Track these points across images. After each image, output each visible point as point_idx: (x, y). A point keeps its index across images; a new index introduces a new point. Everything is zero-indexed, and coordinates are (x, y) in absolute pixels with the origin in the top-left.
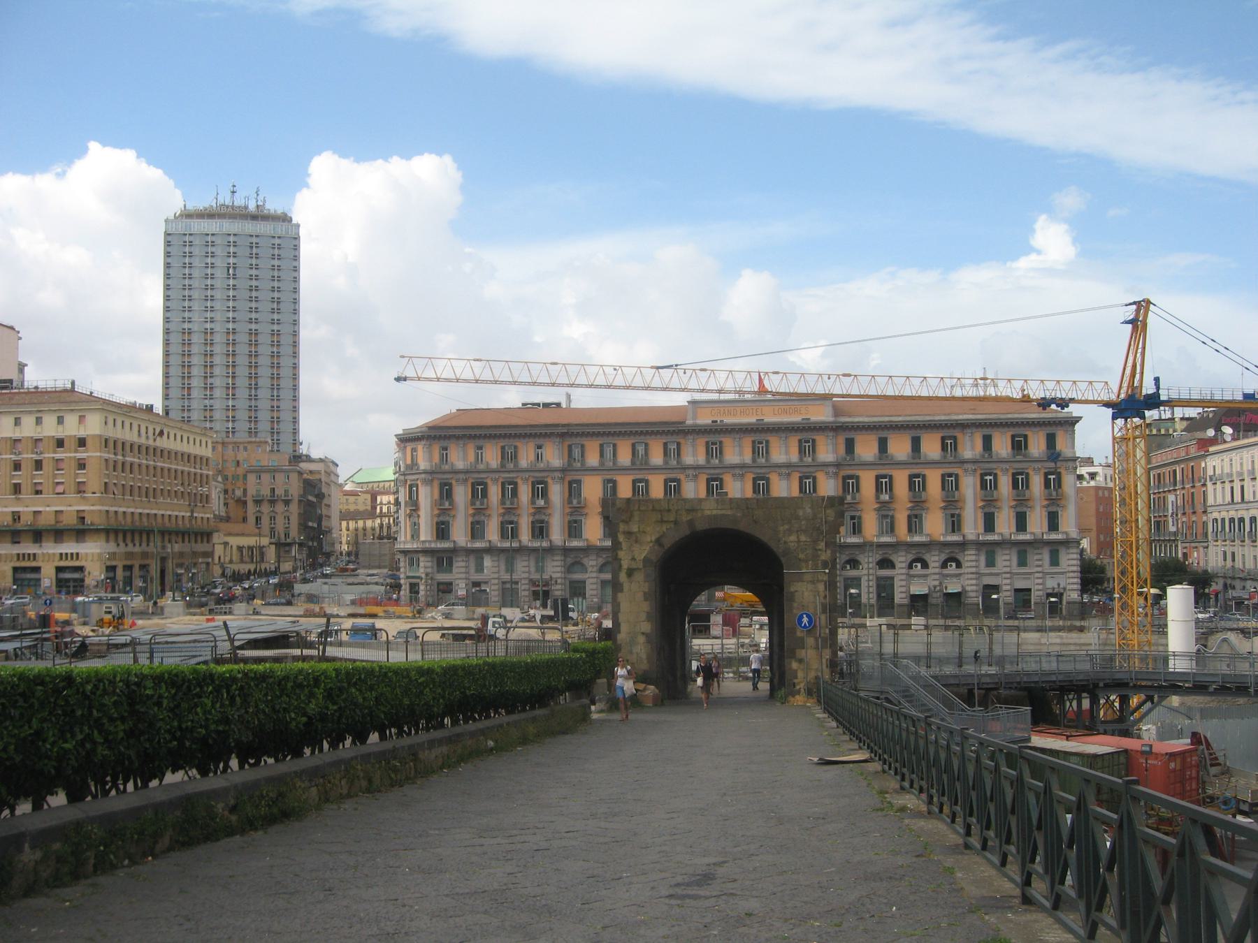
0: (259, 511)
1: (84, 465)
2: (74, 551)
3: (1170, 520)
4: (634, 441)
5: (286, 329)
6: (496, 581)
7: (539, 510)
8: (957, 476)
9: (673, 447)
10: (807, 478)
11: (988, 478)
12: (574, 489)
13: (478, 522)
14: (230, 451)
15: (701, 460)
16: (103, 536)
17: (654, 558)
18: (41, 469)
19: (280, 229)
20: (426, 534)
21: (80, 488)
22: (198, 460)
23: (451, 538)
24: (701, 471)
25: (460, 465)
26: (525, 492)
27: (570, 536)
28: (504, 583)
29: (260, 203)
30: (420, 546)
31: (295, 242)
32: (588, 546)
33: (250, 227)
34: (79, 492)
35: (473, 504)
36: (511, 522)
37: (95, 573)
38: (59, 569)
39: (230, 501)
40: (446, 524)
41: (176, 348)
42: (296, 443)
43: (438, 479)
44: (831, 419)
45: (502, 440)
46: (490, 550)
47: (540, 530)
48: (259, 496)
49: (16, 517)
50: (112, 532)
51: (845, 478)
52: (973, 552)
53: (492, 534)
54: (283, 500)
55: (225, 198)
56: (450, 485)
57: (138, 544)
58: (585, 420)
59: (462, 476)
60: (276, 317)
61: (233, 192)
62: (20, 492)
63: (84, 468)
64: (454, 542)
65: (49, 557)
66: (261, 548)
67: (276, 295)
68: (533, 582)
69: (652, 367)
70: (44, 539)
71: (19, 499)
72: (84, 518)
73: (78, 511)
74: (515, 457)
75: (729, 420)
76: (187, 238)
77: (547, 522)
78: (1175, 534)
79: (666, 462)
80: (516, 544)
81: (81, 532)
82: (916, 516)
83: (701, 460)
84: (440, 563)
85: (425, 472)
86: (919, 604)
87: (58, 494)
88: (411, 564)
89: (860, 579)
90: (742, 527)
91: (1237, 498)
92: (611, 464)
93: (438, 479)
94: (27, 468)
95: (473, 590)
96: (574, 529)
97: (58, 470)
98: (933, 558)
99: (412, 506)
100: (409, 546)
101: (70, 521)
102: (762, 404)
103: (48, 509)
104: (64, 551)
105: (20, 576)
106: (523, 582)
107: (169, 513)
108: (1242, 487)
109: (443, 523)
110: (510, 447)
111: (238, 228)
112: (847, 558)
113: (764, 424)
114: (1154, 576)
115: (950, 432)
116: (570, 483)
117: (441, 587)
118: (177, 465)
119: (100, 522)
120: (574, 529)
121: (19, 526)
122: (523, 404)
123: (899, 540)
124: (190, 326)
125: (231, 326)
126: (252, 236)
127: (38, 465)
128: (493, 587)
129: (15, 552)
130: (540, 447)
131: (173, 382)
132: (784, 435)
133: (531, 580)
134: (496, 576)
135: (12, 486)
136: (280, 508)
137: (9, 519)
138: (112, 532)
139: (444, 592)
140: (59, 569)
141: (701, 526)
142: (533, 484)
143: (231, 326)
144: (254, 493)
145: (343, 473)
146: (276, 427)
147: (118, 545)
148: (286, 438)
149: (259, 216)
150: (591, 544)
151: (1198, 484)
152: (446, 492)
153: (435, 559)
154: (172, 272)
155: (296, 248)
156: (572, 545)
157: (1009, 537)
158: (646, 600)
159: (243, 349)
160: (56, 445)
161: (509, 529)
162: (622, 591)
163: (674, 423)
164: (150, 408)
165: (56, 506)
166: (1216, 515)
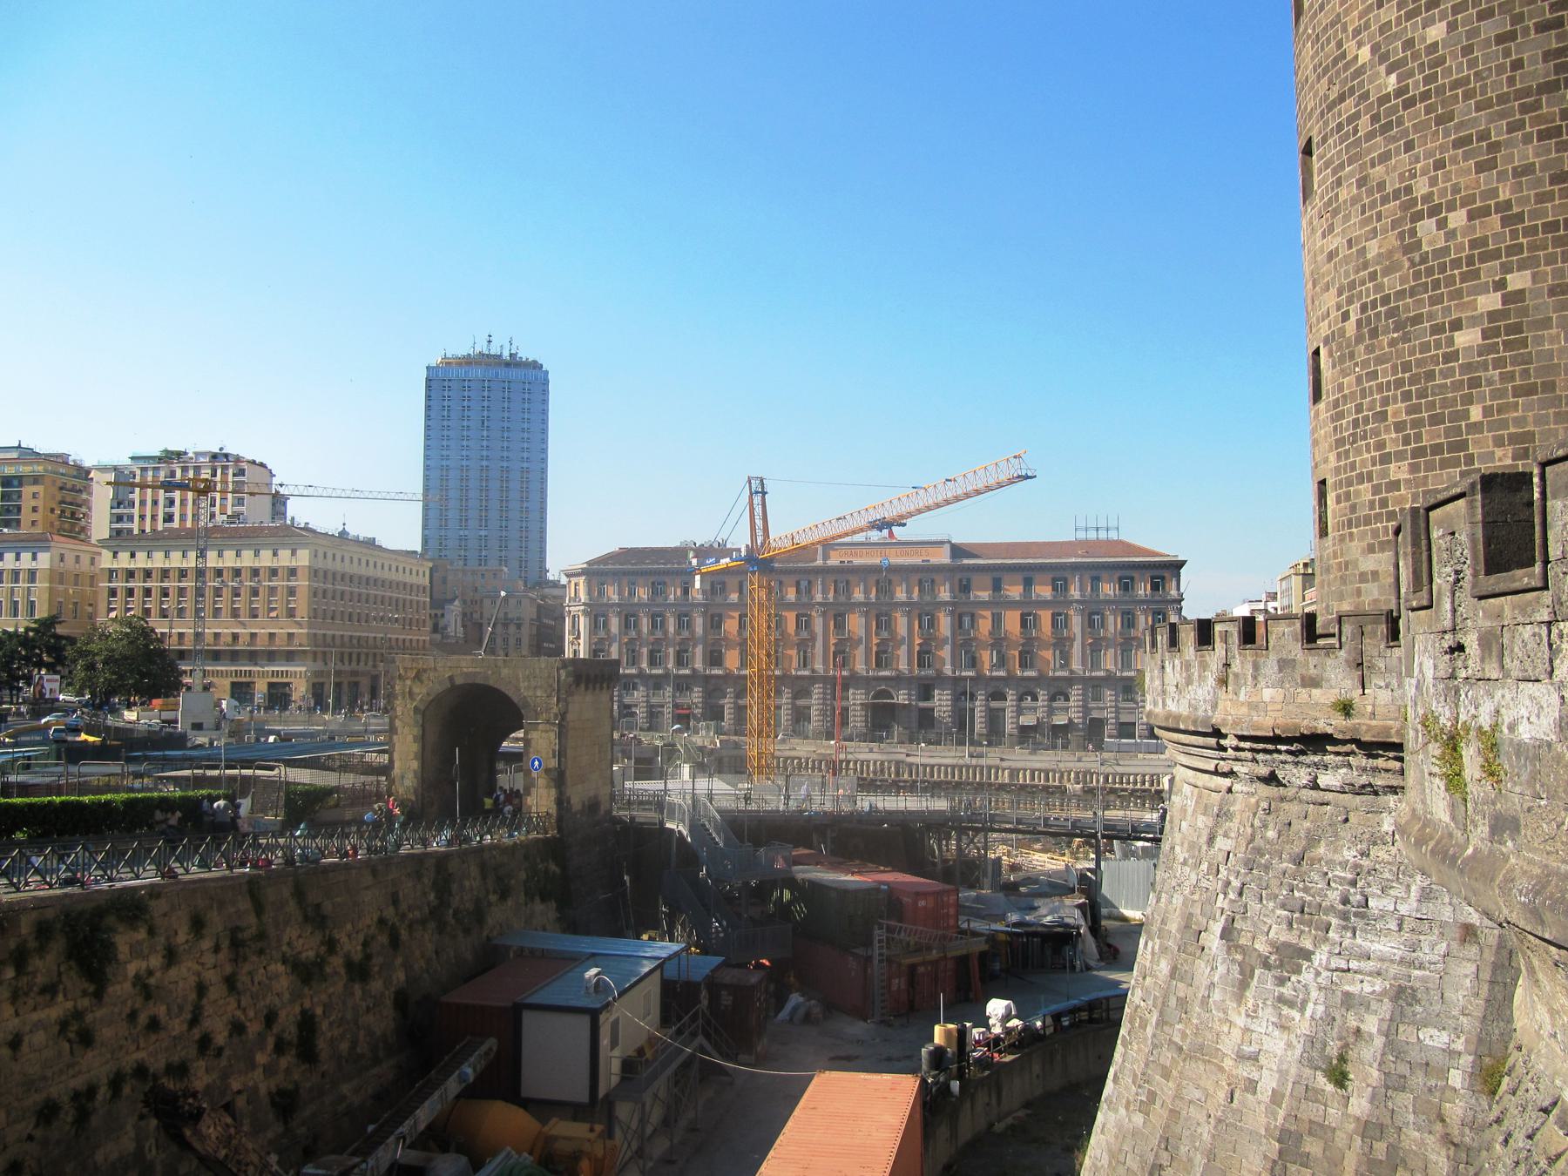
9: (804, 584)
11: (1096, 617)
19: (531, 373)
33: (503, 373)
37: (300, 690)
38: (271, 685)
39: (469, 623)
51: (712, 616)
55: (481, 347)
57: (347, 663)
76: (446, 384)
82: (1028, 652)
86: (1025, 734)
90: (491, 683)
114: (587, 688)
115: (1059, 576)
116: (712, 616)
124: (448, 463)
125: (484, 463)
136: (512, 629)
137: (230, 639)
140: (271, 685)
143: (484, 463)
149: (514, 363)
154: (433, 414)
155: (545, 392)
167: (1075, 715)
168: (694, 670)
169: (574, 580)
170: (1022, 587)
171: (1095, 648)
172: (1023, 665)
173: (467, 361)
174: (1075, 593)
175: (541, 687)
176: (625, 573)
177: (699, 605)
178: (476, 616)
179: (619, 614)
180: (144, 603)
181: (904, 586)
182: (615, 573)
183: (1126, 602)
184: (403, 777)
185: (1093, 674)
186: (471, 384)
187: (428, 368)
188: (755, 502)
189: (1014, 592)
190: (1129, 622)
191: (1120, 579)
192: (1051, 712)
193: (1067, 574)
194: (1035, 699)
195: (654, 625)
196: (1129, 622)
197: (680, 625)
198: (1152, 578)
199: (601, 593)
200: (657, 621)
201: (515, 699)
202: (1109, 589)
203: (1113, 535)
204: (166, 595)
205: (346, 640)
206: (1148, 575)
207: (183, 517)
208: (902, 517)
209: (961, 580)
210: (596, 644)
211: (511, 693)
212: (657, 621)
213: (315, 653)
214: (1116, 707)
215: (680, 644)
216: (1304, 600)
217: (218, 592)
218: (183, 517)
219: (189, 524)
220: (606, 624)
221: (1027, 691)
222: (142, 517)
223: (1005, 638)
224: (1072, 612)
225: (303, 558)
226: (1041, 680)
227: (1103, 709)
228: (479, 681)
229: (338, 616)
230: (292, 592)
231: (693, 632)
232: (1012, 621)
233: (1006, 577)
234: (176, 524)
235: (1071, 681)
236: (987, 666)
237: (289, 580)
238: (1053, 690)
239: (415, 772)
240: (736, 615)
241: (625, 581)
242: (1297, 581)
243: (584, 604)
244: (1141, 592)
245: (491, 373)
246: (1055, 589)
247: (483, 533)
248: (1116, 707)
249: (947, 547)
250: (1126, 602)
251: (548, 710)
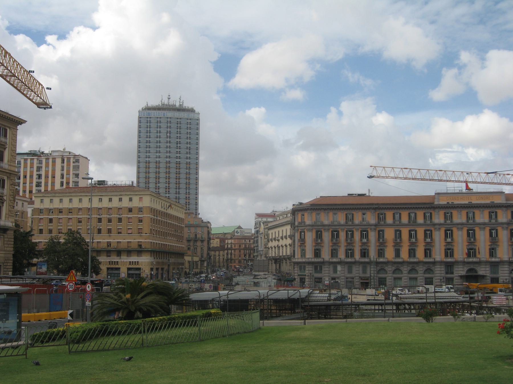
0: (189, 245)
1: (142, 220)
2: (136, 261)
4: (409, 212)
6: (343, 278)
7: (364, 244)
8: (431, 231)
9: (397, 216)
10: (493, 230)
12: (381, 234)
13: (335, 249)
15: (442, 221)
16: (149, 253)
18: (121, 222)
19: (191, 115)
20: (309, 255)
21: (140, 231)
22: (180, 219)
23: (321, 257)
24: (442, 226)
25: (326, 222)
26: (357, 236)
27: (379, 256)
28: (347, 278)
29: (181, 104)
30: (307, 260)
31: (197, 121)
32: (388, 261)
33: (177, 114)
34: (139, 233)
35: (332, 241)
36: (350, 250)
38: (129, 269)
40: (319, 250)
43: (315, 229)
44: (505, 202)
45: (346, 211)
46: (340, 263)
47: (364, 253)
48: (189, 238)
49: (109, 244)
50: (155, 252)
52: (461, 267)
53: (342, 255)
54: (200, 240)
56: (321, 232)
58: (403, 202)
59: (327, 227)
60: (188, 156)
61: (169, 98)
62: (111, 233)
63: (142, 222)
64: (323, 259)
65: (124, 263)
67: (188, 146)
68: (361, 278)
69: (485, 173)
70: (122, 255)
71: (110, 236)
72: (141, 245)
73: (138, 242)
75: (456, 202)
76: (149, 119)
77: (368, 250)
79: (425, 222)
80: (353, 260)
81: (140, 251)
83: (442, 221)
84: (316, 268)
85: (309, 225)
87: (129, 234)
88: (300, 269)
89: (453, 278)
92: (398, 222)
93: (315, 229)
94: (115, 222)
95: (332, 282)
96: (381, 253)
97: (129, 223)
98: (420, 269)
99: (302, 241)
100: (300, 260)
101: (134, 246)
102: (471, 194)
103: (124, 241)
104: (131, 261)
105: (130, 272)
106: (356, 278)
109: (317, 250)
110: (350, 214)
111: (172, 115)
112: (380, 268)
113: (495, 204)
116: (379, 231)
117: (316, 280)
118: (173, 222)
119: (149, 247)
120: (381, 253)
121: (109, 248)
122: (348, 195)
123: (456, 260)
124: (150, 159)
126: (178, 118)
127: (120, 220)
128: (342, 280)
129: (108, 261)
130: (364, 214)
132: (459, 210)
133: (360, 277)
134: (343, 275)
135: (107, 230)
136: (199, 244)
137: (106, 245)
138: (155, 252)
139: (317, 282)
140: (129, 269)
142: (361, 231)
144: (187, 237)
146: (188, 206)
147: (155, 258)
149: (181, 109)
150: (389, 260)
152: (319, 235)
153: (314, 267)
155: (198, 124)
156: (448, 260)
157: (358, 260)
159: (173, 170)
160: (128, 211)
161: (349, 253)
163: (428, 203)
165: (118, 239)
186: (151, 119)
222: (47, 177)
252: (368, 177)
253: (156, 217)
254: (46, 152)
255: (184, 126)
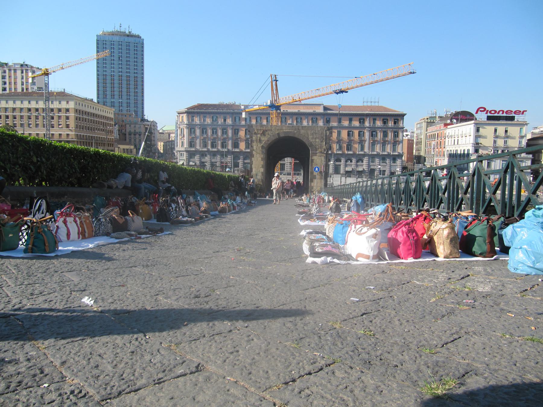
3: (432, 150)
5: (139, 76)
9: (259, 119)
11: (374, 133)
14: (120, 117)
17: (265, 146)
33: (127, 39)
39: (121, 134)
41: (101, 81)
42: (143, 115)
51: (235, 130)
55: (118, 29)
66: (131, 150)
74: (216, 120)
78: (434, 155)
88: (181, 155)
90: (296, 136)
91: (456, 143)
107: (99, 136)
108: (458, 140)
115: (362, 118)
116: (235, 130)
124: (106, 73)
125: (120, 74)
131: (100, 92)
136: (137, 136)
141: (282, 135)
145: (159, 128)
148: (140, 113)
149: (130, 35)
151: (443, 139)
158: (262, 160)
162: (253, 157)
164: (92, 100)
166: (448, 149)
167: (365, 167)
168: (228, 149)
169: (181, 115)
170: (348, 122)
171: (373, 144)
172: (348, 150)
173: (113, 34)
174: (367, 124)
175: (318, 138)
176: (202, 113)
177: (230, 125)
178: (123, 131)
179: (200, 128)
180: (6, 121)
181: (306, 120)
182: (198, 113)
183: (385, 128)
184: (257, 175)
185: (373, 153)
187: (97, 36)
188: (273, 84)
189: (346, 123)
190: (385, 135)
191: (383, 120)
192: (357, 166)
193: (364, 117)
194: (351, 161)
195: (213, 133)
196: (385, 135)
197: (223, 133)
198: (394, 120)
199: (193, 120)
200: (214, 131)
201: (307, 143)
202: (379, 123)
203: (377, 104)
204: (15, 118)
205: (88, 137)
206: (393, 118)
207: (10, 89)
208: (348, 89)
209: (327, 119)
210: (191, 139)
211: (304, 140)
212: (214, 131)
213: (77, 142)
214: (390, 165)
215: (223, 140)
216: (427, 131)
217: (37, 117)
218: (10, 89)
219: (13, 91)
220: (194, 132)
221: (349, 159)
222: (10, 83)
223: (342, 140)
224: (366, 131)
225: (71, 105)
226: (354, 155)
227: (375, 165)
228: (291, 135)
229: (84, 128)
230: (67, 118)
231: (228, 135)
232: (344, 134)
233: (343, 118)
234: (8, 91)
235: (364, 155)
236: (335, 150)
237: (66, 113)
238: (358, 159)
239: (262, 173)
240: (244, 129)
241: (202, 116)
242: (424, 125)
243: (186, 124)
244: (390, 125)
245: (122, 39)
246: (360, 122)
247: (120, 100)
248: (390, 165)
249: (322, 107)
250: (385, 128)
251: (321, 147)
252: (526, 111)
253: (81, 116)
254: (10, 64)
255: (132, 48)
